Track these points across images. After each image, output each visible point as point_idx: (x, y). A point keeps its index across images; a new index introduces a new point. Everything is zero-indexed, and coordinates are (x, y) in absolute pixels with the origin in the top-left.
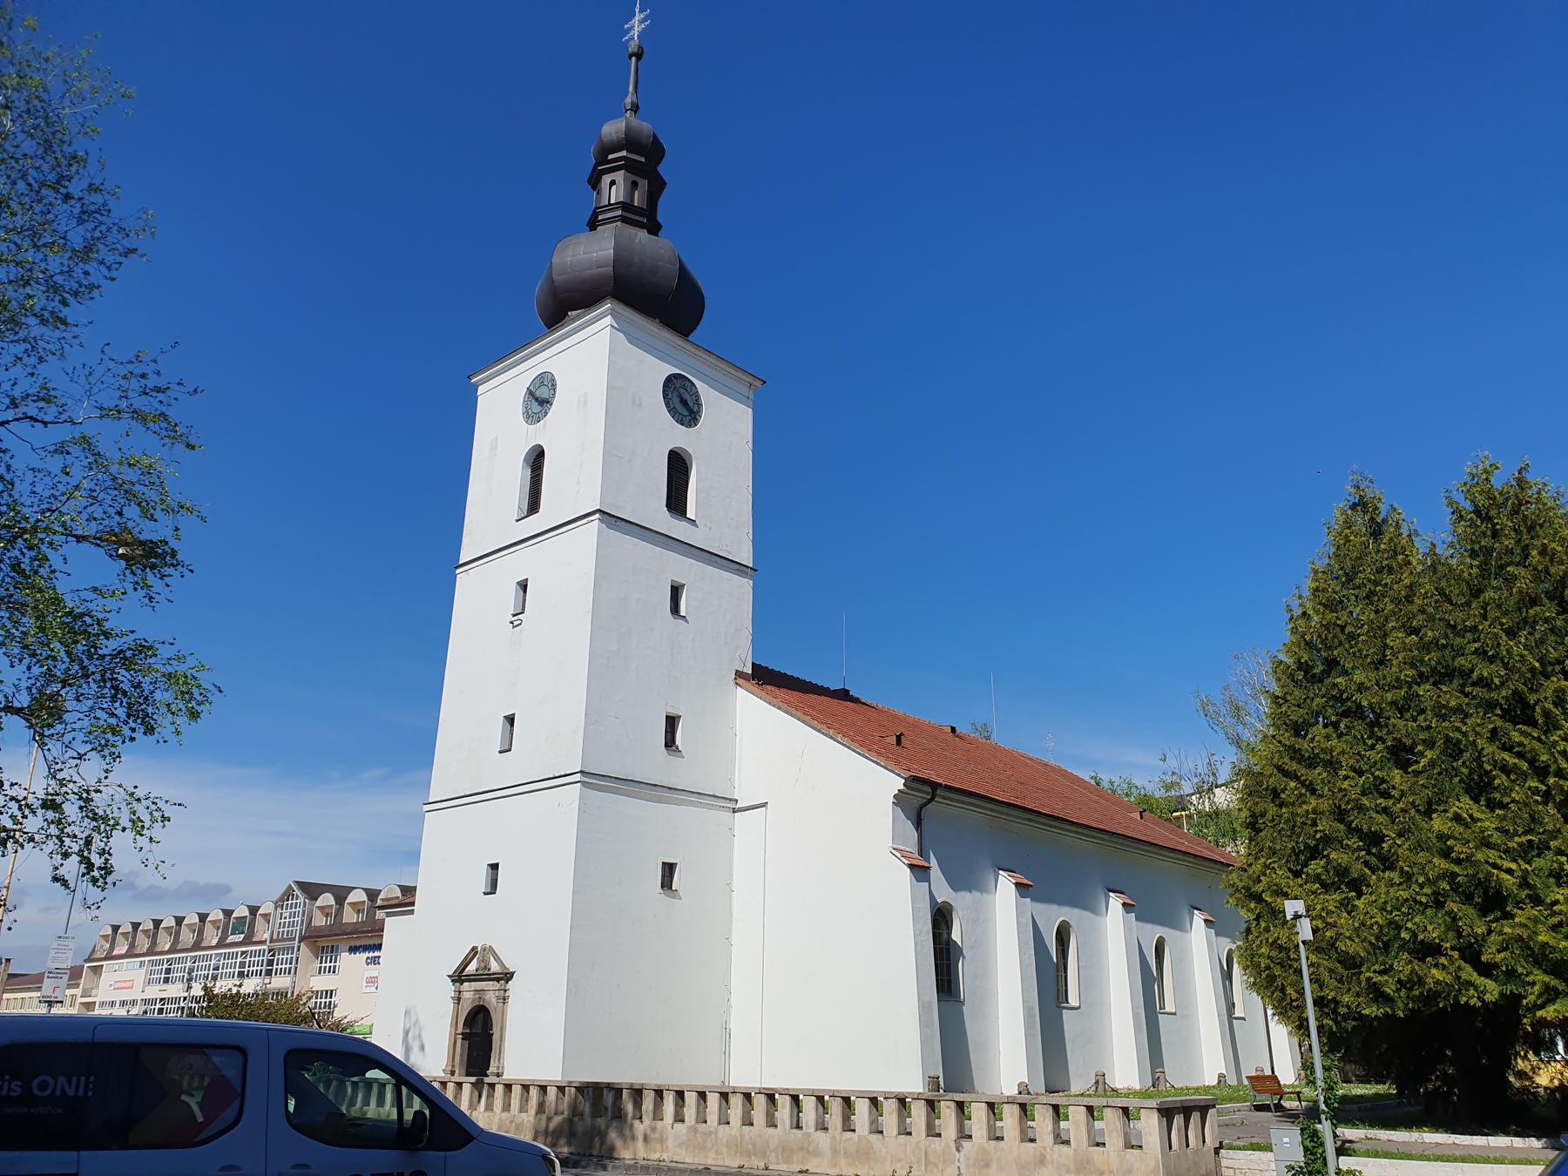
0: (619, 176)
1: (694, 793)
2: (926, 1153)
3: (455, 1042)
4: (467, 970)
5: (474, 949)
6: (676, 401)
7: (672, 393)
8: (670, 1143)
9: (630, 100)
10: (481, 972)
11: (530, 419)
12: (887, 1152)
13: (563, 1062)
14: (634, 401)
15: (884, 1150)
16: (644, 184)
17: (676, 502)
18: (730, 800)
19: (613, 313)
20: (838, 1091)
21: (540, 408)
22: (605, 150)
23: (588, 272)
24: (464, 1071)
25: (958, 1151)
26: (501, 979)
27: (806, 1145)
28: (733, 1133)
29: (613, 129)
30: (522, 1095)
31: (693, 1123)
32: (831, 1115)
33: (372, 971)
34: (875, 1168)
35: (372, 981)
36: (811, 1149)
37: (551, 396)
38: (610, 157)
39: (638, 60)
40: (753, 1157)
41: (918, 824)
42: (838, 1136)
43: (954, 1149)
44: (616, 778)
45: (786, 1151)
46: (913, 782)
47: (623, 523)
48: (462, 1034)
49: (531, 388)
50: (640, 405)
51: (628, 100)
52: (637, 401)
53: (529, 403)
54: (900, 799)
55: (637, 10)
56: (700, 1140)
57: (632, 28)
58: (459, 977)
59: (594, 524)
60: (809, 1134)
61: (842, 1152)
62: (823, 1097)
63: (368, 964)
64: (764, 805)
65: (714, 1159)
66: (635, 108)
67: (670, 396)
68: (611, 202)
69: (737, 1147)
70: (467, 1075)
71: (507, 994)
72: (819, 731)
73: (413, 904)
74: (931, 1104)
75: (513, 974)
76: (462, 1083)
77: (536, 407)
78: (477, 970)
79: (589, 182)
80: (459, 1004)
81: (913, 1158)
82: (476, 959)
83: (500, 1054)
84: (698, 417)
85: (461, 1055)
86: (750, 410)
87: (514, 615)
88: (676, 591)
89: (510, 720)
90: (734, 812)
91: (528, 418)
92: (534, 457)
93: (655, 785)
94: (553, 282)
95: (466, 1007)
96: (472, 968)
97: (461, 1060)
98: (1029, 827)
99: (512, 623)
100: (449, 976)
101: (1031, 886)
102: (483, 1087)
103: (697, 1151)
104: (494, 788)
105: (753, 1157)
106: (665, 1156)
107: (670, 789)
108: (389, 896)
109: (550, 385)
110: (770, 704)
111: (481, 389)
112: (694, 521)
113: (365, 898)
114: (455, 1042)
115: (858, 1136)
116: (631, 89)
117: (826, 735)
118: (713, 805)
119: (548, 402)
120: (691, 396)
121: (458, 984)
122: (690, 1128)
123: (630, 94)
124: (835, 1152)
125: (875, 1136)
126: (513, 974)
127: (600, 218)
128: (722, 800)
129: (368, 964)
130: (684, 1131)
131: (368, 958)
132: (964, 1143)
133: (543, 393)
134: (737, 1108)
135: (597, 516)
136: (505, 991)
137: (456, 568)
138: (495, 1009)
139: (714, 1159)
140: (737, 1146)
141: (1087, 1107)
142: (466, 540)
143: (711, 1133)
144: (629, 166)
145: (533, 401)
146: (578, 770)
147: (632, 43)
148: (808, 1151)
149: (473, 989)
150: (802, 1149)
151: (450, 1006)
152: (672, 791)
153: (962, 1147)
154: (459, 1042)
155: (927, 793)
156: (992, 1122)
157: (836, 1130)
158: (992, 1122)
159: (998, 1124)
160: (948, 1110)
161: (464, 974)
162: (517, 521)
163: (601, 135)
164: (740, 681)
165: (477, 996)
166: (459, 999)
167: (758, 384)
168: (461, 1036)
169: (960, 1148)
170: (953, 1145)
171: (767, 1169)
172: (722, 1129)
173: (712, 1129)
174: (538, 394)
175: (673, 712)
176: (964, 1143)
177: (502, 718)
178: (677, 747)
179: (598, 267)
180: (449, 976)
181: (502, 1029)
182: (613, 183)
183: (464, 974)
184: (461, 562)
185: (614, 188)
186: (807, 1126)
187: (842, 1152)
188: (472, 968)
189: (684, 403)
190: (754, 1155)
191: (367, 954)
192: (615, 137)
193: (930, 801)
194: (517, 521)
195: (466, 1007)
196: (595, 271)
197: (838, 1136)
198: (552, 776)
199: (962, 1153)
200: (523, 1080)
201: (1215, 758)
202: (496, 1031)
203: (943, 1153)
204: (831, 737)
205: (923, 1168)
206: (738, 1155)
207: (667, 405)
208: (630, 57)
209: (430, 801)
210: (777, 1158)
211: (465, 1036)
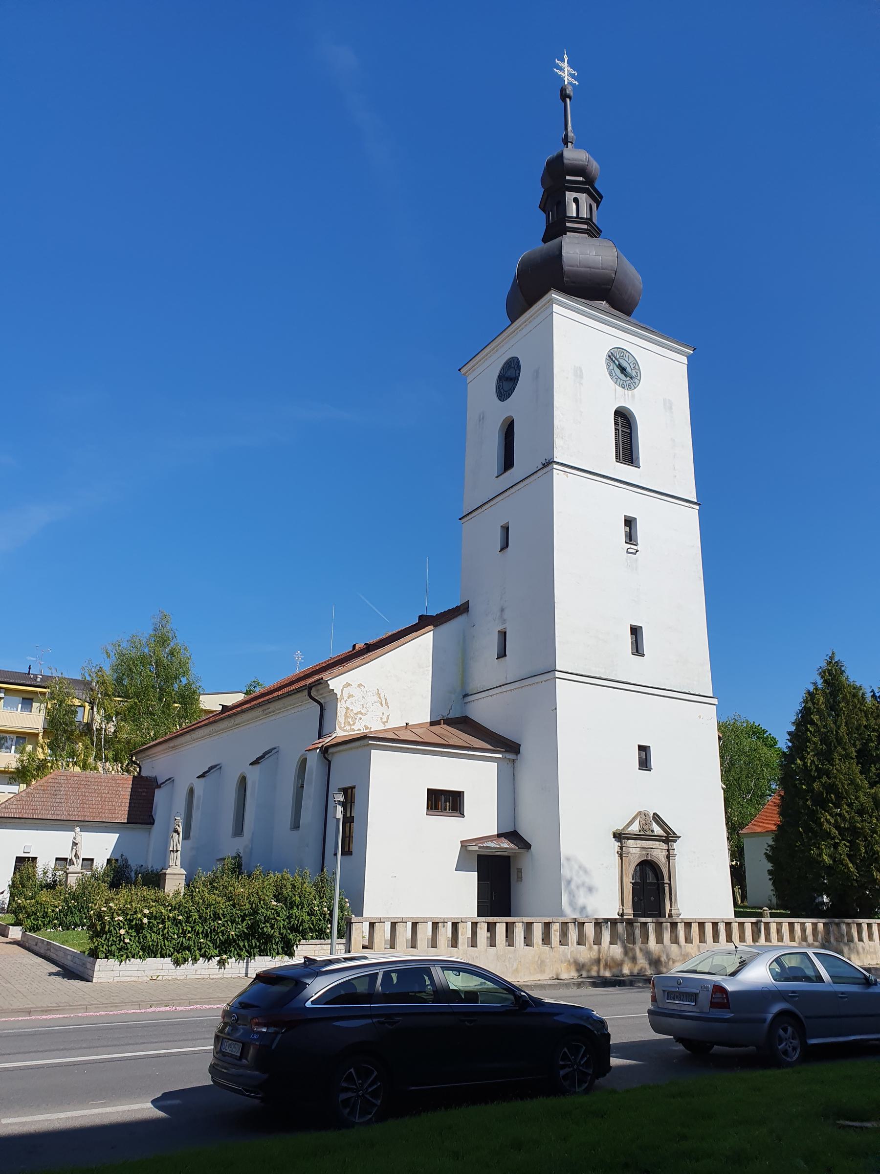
4: (629, 829)
188: (635, 828)
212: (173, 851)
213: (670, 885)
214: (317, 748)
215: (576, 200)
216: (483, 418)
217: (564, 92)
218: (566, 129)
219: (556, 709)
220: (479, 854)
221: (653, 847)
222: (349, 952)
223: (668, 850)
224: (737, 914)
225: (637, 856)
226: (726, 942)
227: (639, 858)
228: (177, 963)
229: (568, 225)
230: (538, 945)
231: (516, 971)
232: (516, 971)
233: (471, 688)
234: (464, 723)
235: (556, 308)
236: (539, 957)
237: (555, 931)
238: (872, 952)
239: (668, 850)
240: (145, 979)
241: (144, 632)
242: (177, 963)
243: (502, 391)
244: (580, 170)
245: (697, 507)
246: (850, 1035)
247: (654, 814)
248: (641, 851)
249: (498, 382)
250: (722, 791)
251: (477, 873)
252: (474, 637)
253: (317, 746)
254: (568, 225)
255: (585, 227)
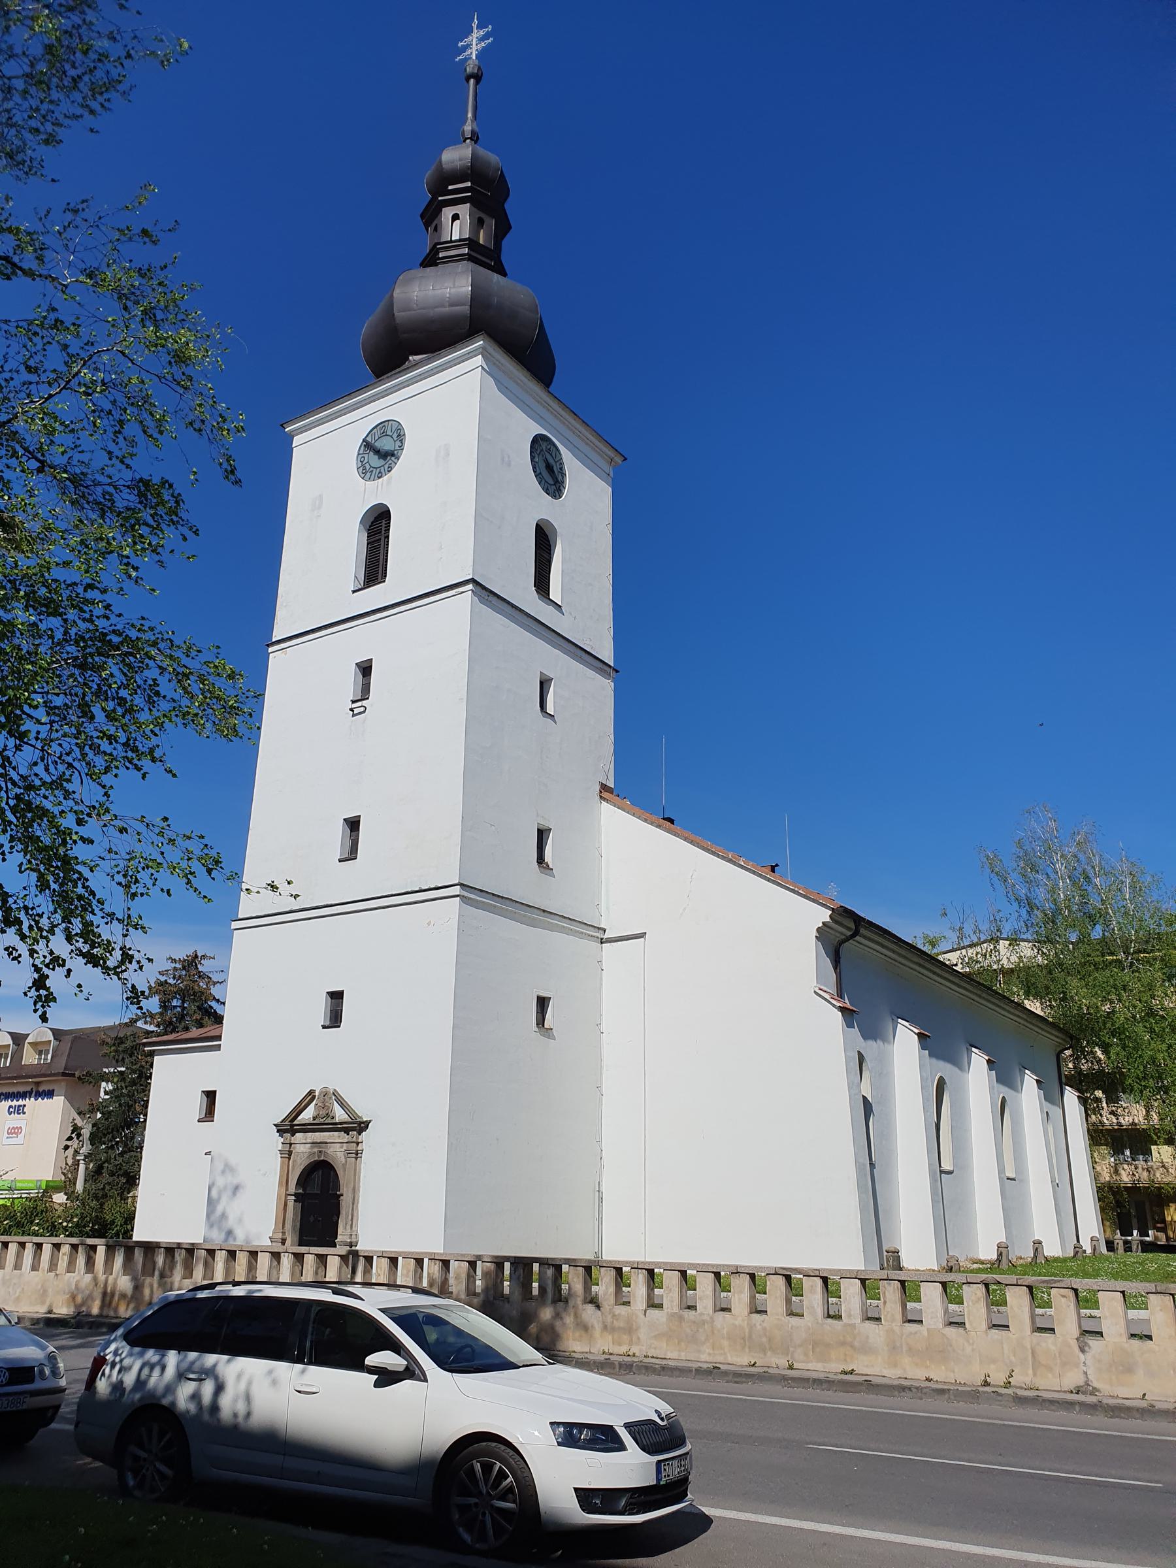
0: (464, 210)
1: (565, 918)
2: (1033, 1353)
3: (286, 1205)
4: (299, 1118)
5: (311, 1092)
6: (542, 465)
7: (539, 455)
8: (643, 1334)
9: (470, 128)
10: (322, 1121)
11: (368, 474)
12: (973, 1350)
13: (445, 1231)
14: (503, 460)
15: (968, 1349)
16: (491, 223)
17: (542, 583)
18: (599, 928)
19: (484, 352)
20: (386, 1252)
21: (382, 462)
22: (442, 182)
23: (438, 310)
24: (296, 1239)
25: (1083, 1351)
26: (353, 1129)
27: (849, 1339)
28: (737, 1323)
29: (456, 156)
30: (416, 1272)
31: (676, 1309)
32: (885, 1302)
33: (16, 1120)
34: (956, 1370)
35: (15, 1131)
36: (856, 1344)
37: (397, 448)
38: (450, 187)
39: (477, 82)
40: (769, 1353)
41: (836, 962)
42: (897, 1329)
43: (1077, 1350)
44: (493, 895)
45: (818, 1345)
46: (843, 914)
47: (495, 598)
48: (295, 1195)
49: (369, 439)
50: (509, 465)
51: (468, 128)
52: (506, 459)
53: (366, 456)
54: (823, 933)
55: (475, 26)
56: (688, 1331)
57: (469, 46)
58: (288, 1127)
59: (466, 598)
60: (853, 1326)
61: (905, 1348)
62: (653, 1270)
63: (10, 1113)
64: (642, 935)
65: (709, 1354)
66: (475, 138)
67: (536, 460)
68: (453, 239)
69: (746, 1340)
70: (300, 1245)
71: (359, 1148)
72: (713, 853)
73: (219, 1038)
74: (276, 1256)
75: (367, 1124)
76: (42, 1244)
77: (375, 461)
78: (314, 1119)
79: (422, 216)
80: (289, 1159)
81: (1013, 1359)
82: (313, 1105)
83: (352, 1220)
84: (562, 488)
85: (294, 1220)
86: (610, 489)
87: (353, 702)
88: (544, 684)
89: (353, 824)
90: (602, 943)
91: (366, 473)
92: (372, 519)
93: (530, 906)
94: (394, 319)
95: (299, 1162)
96: (307, 1115)
97: (294, 1227)
98: (915, 973)
99: (352, 710)
100: (275, 1125)
101: (929, 1036)
102: (358, 1260)
103: (683, 1344)
104: (333, 903)
105: (769, 1353)
106: (635, 1349)
107: (544, 911)
108: (39, 1040)
109: (395, 436)
110: (646, 821)
111: (297, 440)
112: (560, 606)
113: (11, 1042)
114: (286, 1205)
115: (928, 1329)
116: (470, 115)
117: (723, 858)
118: (582, 933)
119: (393, 455)
120: (556, 462)
121: (288, 1135)
122: (672, 1316)
123: (469, 121)
124: (894, 1348)
125: (952, 1332)
126: (367, 1124)
127: (441, 255)
128: (591, 928)
129: (10, 1113)
130: (664, 1320)
131: (10, 1107)
132: (1090, 1342)
133: (386, 444)
134: (741, 1292)
135: (470, 586)
136: (358, 1143)
137: (268, 646)
138: (344, 1165)
139: (709, 1354)
140: (744, 1339)
141: (19, 1243)
142: (280, 613)
143: (704, 1322)
144: (476, 201)
145: (371, 453)
146: (457, 882)
147: (470, 62)
148: (852, 1347)
149: (309, 1141)
150: (843, 1344)
151: (275, 1163)
152: (546, 914)
153: (1090, 1347)
154: (291, 1204)
155: (849, 929)
156: (684, 1291)
157: (893, 1320)
158: (684, 1291)
159: (594, 1288)
160: (1063, 1300)
161: (295, 1122)
162: (354, 592)
163: (440, 161)
164: (605, 795)
165: (316, 1150)
166: (290, 1153)
167: (619, 460)
168: (293, 1197)
169: (1086, 1349)
170: (1074, 1345)
171: (791, 1367)
172: (721, 1319)
173: (705, 1317)
174: (378, 445)
175: (546, 824)
176: (1090, 1342)
177: (342, 821)
178: (547, 864)
179: (451, 305)
180: (275, 1125)
181: (355, 1190)
182: (456, 217)
183: (295, 1122)
184: (274, 640)
185: (457, 223)
186: (849, 1316)
187: (905, 1348)
188: (307, 1115)
189: (549, 468)
190: (771, 1348)
191: (9, 1103)
192: (458, 164)
193: (853, 936)
194: (354, 592)
195: (299, 1162)
196: (447, 310)
197: (897, 1329)
198: (417, 889)
199: (1089, 1355)
200: (392, 1252)
201: (1001, 914)
202: (345, 1190)
203: (1060, 1353)
204: (730, 861)
205: (1030, 1372)
206: (747, 1350)
207: (534, 468)
208: (468, 80)
209: (240, 916)
210: (806, 1355)
211: (298, 1198)
221: (328, 1141)
225: (306, 1155)
226: (746, 1311)
227: (308, 1157)
230: (893, 1320)
231: (18, 1299)
232: (18, 1299)
236: (42, 1286)
237: (63, 1254)
238: (619, 1328)
243: (367, 466)
248: (312, 1148)
249: (361, 452)
250: (916, 1036)
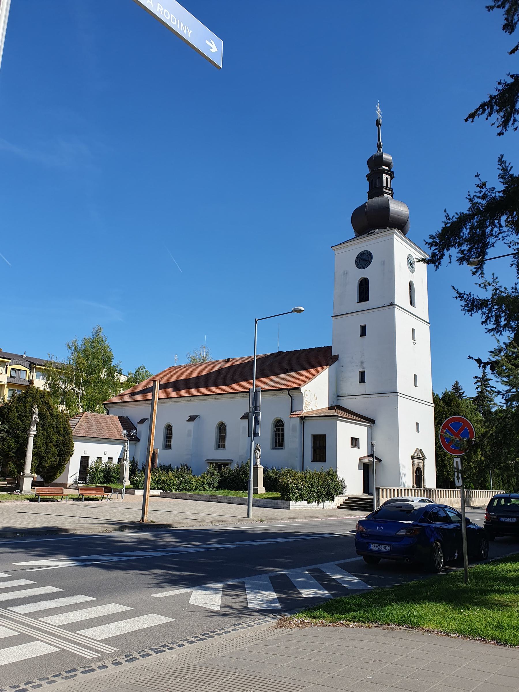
212: (258, 458)
213: (424, 476)
214: (299, 417)
215: (387, 178)
216: (347, 273)
217: (378, 122)
218: (379, 140)
219: (398, 408)
220: (364, 463)
222: (253, 506)
223: (423, 463)
224: (437, 488)
228: (308, 503)
229: (384, 190)
233: (341, 393)
234: (339, 407)
235: (395, 236)
239: (423, 463)
240: (301, 509)
241: (89, 335)
242: (308, 503)
243: (360, 265)
244: (388, 164)
245: (429, 325)
246: (273, 567)
247: (420, 449)
251: (363, 471)
252: (343, 371)
253: (299, 416)
254: (384, 190)
255: (390, 192)
